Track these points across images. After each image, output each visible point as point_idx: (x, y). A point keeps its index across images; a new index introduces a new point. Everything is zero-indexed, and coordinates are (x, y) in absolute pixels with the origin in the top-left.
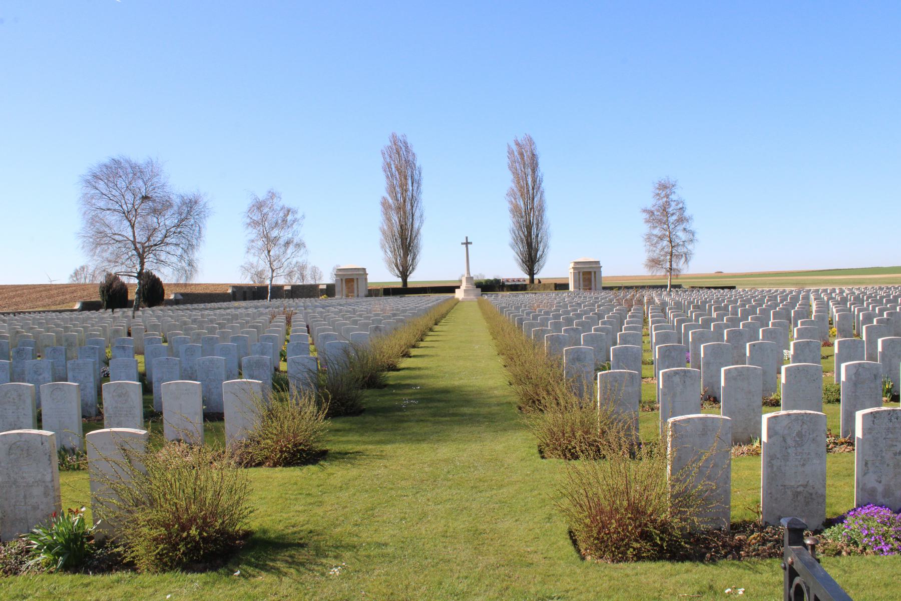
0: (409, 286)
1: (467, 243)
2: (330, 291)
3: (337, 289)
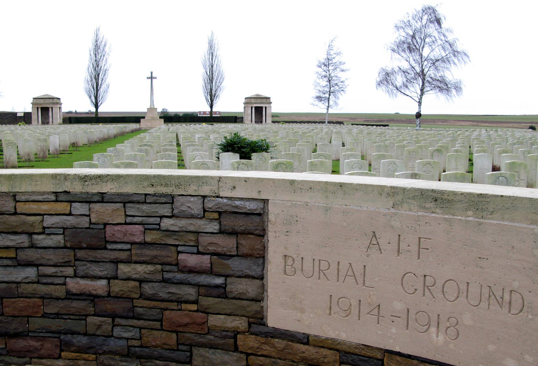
0: (99, 116)
1: (152, 78)
2: (27, 118)
3: (34, 117)
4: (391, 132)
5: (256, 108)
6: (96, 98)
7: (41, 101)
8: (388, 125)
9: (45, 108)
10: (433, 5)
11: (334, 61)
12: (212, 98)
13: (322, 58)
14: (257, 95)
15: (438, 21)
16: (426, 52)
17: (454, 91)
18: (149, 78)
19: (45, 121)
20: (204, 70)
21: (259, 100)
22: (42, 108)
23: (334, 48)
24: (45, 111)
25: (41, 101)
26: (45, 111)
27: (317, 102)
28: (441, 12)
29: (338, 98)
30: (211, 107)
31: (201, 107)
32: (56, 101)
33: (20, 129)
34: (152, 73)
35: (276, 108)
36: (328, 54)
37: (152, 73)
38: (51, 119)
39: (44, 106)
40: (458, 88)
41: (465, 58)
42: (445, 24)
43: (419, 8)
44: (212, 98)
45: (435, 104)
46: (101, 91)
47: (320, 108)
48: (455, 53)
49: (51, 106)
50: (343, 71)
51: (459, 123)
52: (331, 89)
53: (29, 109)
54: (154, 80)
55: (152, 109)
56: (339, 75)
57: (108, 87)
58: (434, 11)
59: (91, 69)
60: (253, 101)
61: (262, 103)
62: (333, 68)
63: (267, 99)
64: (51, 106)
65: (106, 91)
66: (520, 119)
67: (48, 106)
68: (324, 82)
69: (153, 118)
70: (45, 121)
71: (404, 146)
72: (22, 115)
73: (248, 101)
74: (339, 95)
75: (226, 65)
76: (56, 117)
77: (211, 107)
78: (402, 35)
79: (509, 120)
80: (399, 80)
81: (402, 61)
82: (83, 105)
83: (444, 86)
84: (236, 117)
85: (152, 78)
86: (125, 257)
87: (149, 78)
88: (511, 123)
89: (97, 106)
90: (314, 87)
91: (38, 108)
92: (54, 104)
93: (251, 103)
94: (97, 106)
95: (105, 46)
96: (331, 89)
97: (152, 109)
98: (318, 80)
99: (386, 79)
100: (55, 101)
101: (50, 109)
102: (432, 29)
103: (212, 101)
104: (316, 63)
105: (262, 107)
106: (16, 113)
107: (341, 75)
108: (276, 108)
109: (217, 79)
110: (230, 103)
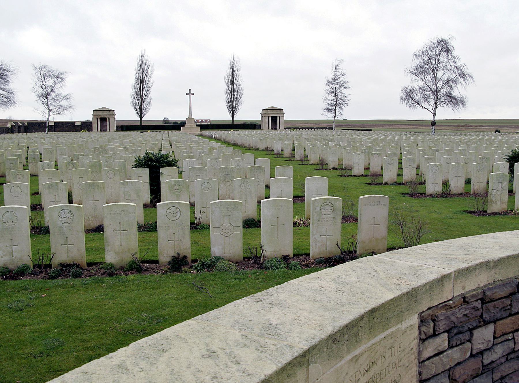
1: (190, 94)
2: (86, 126)
3: (94, 126)
4: (375, 134)
5: (272, 117)
6: (141, 110)
7: (100, 113)
8: (371, 130)
9: (103, 118)
10: (445, 37)
11: (339, 80)
12: (233, 110)
13: (330, 77)
14: (272, 107)
15: (448, 51)
16: (439, 75)
17: (460, 104)
18: (188, 94)
19: (103, 129)
20: (226, 87)
21: (274, 112)
22: (100, 118)
23: (340, 71)
24: (103, 120)
25: (100, 113)
26: (103, 120)
27: (326, 113)
28: (453, 43)
29: (342, 109)
30: (233, 117)
31: (225, 116)
32: (111, 112)
33: (84, 135)
34: (190, 90)
35: (289, 116)
36: (335, 75)
37: (190, 90)
38: (108, 127)
39: (102, 117)
40: (463, 103)
41: (469, 79)
42: (455, 53)
43: (435, 41)
44: (233, 110)
45: (446, 113)
46: (144, 104)
47: (330, 117)
48: (463, 75)
49: (108, 116)
50: (346, 88)
51: (403, 127)
52: (337, 102)
53: (90, 118)
54: (191, 96)
55: (190, 119)
56: (343, 91)
57: (150, 101)
58: (446, 43)
59: (137, 87)
60: (269, 112)
61: (277, 114)
62: (338, 86)
63: (281, 111)
64: (108, 116)
65: (149, 103)
66: (496, 123)
67: (106, 117)
68: (331, 97)
69: (191, 127)
70: (103, 129)
71: (469, 145)
72: (53, 124)
73: (265, 112)
74: (343, 107)
75: (245, 82)
76: (281, 126)
77: (233, 117)
78: (417, 62)
79: (441, 124)
80: (418, 96)
81: (417, 83)
82: (132, 117)
83: (455, 101)
84: (255, 125)
85: (190, 94)
86: (108, 234)
87: (188, 94)
88: (442, 126)
89: (141, 117)
90: (323, 101)
91: (97, 119)
92: (110, 115)
93: (268, 114)
94: (141, 117)
95: (148, 68)
96: (337, 102)
97: (190, 119)
98: (327, 96)
99: (409, 95)
100: (111, 112)
101: (108, 119)
102: (443, 57)
103: (233, 112)
104: (325, 81)
105: (277, 117)
106: (75, 122)
107: (345, 91)
108: (289, 116)
109: (237, 95)
110: (247, 113)
